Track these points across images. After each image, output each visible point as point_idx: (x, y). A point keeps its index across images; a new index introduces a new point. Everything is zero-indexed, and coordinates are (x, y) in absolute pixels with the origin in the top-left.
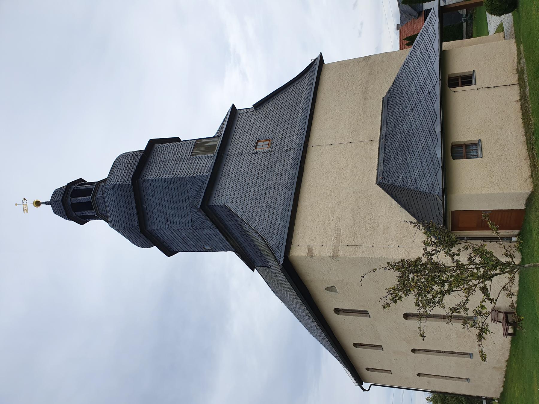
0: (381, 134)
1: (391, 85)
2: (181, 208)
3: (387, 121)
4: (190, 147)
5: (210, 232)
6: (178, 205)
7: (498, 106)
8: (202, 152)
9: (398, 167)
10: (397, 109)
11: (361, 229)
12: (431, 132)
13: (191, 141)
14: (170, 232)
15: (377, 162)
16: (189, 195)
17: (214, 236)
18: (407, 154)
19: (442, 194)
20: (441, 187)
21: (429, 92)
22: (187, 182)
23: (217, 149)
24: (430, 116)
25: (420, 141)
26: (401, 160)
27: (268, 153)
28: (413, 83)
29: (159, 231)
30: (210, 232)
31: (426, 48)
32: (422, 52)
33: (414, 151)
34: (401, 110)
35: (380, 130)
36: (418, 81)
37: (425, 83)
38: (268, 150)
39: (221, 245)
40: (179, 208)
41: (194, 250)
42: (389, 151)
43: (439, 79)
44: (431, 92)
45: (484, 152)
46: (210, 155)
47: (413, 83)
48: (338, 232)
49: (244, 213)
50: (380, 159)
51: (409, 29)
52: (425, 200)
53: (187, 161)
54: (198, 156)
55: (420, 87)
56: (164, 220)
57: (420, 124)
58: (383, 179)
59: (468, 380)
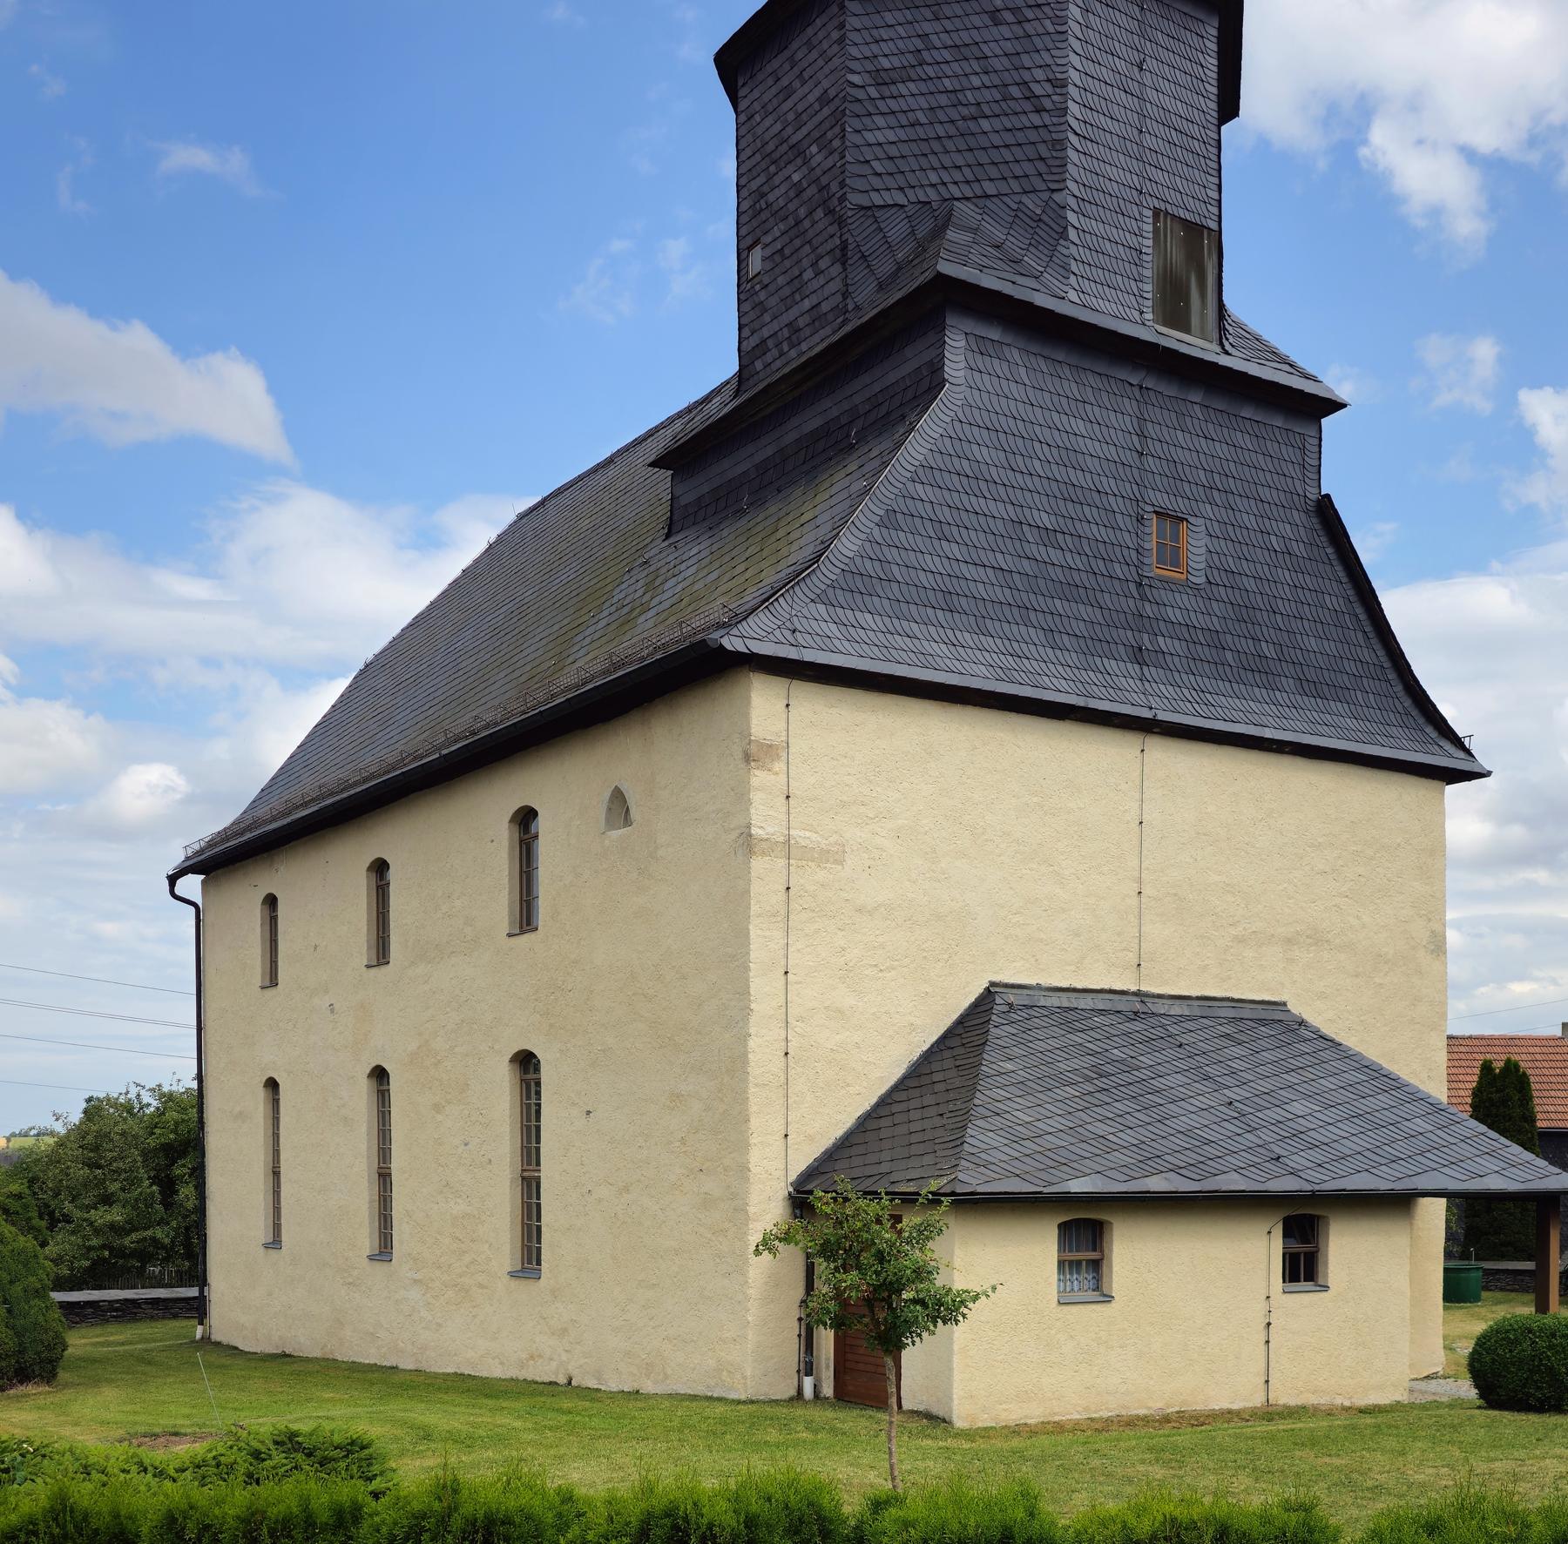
0: (1160, 996)
1: (1327, 1030)
2: (932, 158)
3: (1201, 1020)
4: (1191, 203)
5: (827, 291)
6: (950, 145)
7: (1208, 1350)
8: (1166, 259)
9: (1043, 1057)
10: (1238, 1051)
11: (840, 934)
12: (1149, 1162)
13: (1215, 173)
14: (832, 93)
15: (1065, 984)
16: (988, 203)
17: (807, 304)
18: (1085, 1087)
19: (958, 1191)
20: (980, 1189)
21: (1279, 1157)
22: (1045, 196)
23: (1172, 339)
24: (1202, 1159)
25: (1122, 1128)
26: (1065, 1067)
27: (1133, 568)
28: (1318, 1108)
29: (835, 35)
30: (827, 291)
31: (1430, 1148)
32: (1420, 1137)
33: (1094, 1109)
34: (1234, 1065)
35: (1173, 993)
36: (1321, 1123)
37: (1311, 1146)
38: (1145, 568)
39: (766, 332)
40: (936, 146)
41: (745, 193)
42: (1099, 1025)
43: (1317, 1188)
44: (1278, 1164)
45: (1074, 1309)
46: (1149, 303)
47: (1318, 1108)
48: (831, 856)
49: (909, 475)
50: (1076, 995)
51: (1552, 1072)
52: (936, 1141)
53: (1134, 192)
54: (1150, 243)
55: (1303, 1129)
56: (885, 63)
57: (1178, 1128)
58: (1006, 1008)
59: (275, 1242)
